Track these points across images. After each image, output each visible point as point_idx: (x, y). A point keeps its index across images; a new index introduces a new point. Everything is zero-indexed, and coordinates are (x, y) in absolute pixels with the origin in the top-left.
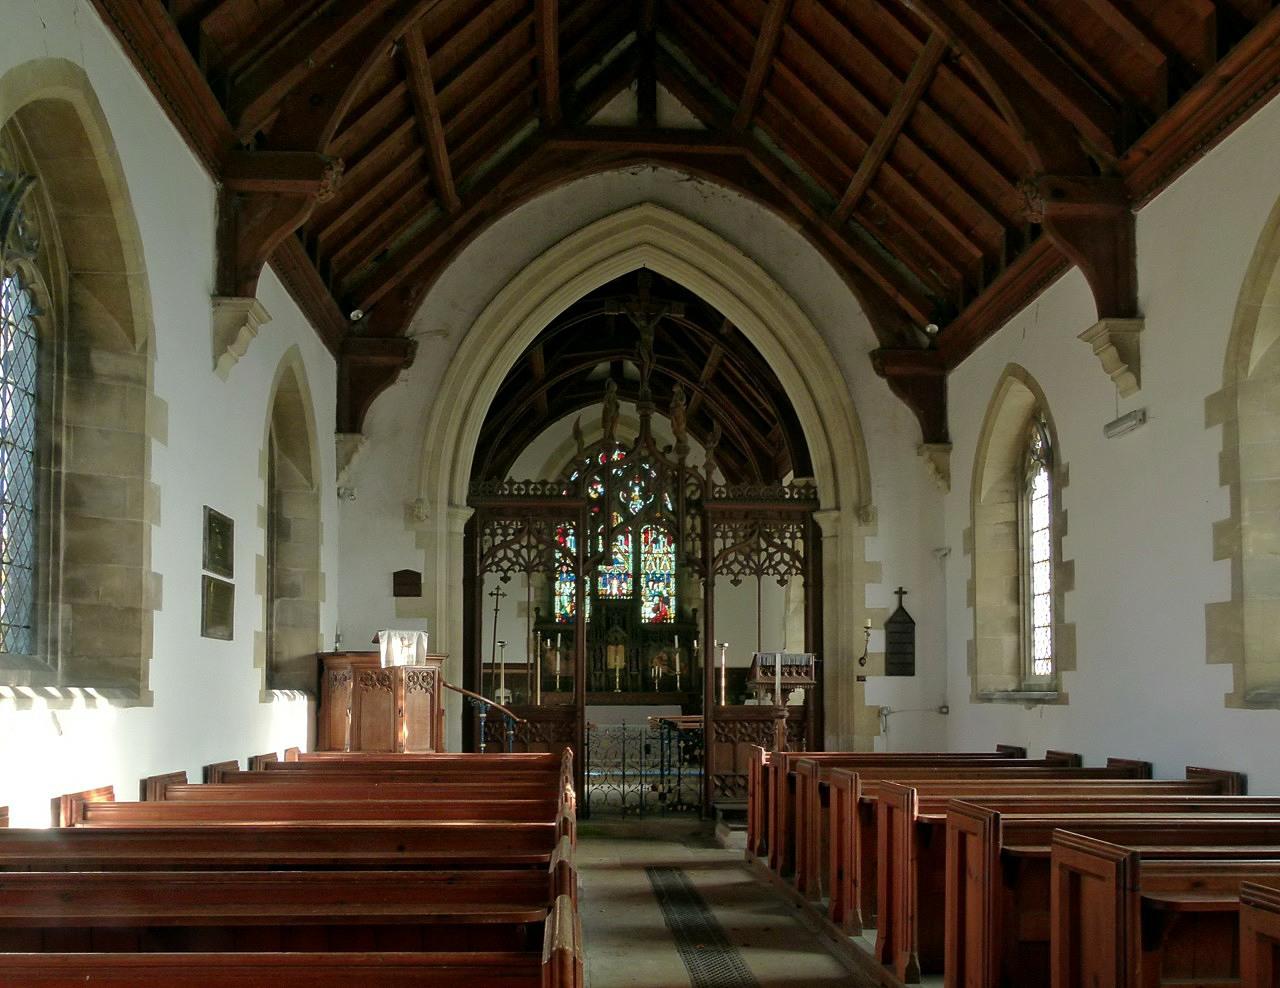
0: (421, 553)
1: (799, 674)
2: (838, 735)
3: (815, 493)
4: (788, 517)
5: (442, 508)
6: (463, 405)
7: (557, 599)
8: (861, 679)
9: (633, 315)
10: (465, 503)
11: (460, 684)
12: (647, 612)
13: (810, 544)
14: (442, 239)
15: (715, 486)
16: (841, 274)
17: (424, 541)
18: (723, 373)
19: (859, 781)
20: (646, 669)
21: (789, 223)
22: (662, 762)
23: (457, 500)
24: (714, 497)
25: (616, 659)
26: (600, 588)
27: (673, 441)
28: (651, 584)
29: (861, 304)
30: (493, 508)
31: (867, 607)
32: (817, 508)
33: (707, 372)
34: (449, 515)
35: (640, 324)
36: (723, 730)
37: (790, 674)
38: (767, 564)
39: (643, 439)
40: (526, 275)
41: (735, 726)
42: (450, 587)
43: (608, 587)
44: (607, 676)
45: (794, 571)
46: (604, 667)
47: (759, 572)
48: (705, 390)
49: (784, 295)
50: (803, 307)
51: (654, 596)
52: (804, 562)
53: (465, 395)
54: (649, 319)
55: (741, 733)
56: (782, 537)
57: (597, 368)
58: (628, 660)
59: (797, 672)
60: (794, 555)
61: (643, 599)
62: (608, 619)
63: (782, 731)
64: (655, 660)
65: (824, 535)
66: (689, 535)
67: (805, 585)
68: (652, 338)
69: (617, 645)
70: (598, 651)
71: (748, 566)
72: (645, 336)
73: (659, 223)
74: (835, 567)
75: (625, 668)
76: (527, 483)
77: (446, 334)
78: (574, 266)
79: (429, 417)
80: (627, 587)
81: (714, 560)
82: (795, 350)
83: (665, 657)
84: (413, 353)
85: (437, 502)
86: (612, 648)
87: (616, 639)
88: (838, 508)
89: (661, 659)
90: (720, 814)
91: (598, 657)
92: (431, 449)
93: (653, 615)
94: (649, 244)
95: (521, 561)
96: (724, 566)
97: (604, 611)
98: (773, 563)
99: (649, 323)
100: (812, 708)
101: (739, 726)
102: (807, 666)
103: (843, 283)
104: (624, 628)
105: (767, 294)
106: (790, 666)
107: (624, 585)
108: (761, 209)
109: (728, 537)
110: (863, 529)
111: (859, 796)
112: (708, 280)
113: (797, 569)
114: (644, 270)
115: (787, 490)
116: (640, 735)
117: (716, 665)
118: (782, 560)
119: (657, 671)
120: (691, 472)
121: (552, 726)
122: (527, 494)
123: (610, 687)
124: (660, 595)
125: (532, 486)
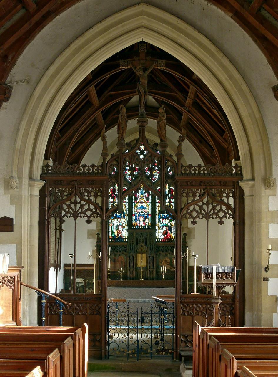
0: (13, 208)
1: (227, 278)
2: (253, 312)
3: (241, 170)
4: (225, 184)
5: (26, 181)
6: (38, 122)
7: (110, 228)
8: (266, 280)
9: (136, 68)
10: (39, 178)
11: (36, 284)
12: (160, 235)
13: (237, 200)
14: (27, 27)
15: (182, 166)
16: (255, 41)
17: (16, 201)
18: (197, 100)
19: (236, 361)
20: (158, 267)
21: (225, 12)
22: (173, 313)
23: (34, 177)
24: (182, 173)
25: (142, 262)
26: (133, 222)
27: (158, 141)
28: (161, 219)
29: (268, 59)
30: (56, 181)
31: (270, 237)
32: (242, 179)
33: (188, 102)
34: (30, 185)
35: (139, 73)
36: (186, 308)
37: (222, 278)
38: (212, 212)
39: (141, 140)
40: (73, 47)
41: (193, 306)
42: (31, 226)
43: (138, 221)
44: (136, 271)
45: (228, 216)
46: (134, 266)
47: (207, 216)
48: (189, 111)
49: (222, 55)
50: (232, 61)
51: (163, 226)
52: (234, 211)
53: (39, 116)
54: (145, 70)
55: (196, 310)
56: (221, 196)
57: (132, 100)
58: (148, 262)
59: (226, 277)
60: (228, 206)
61: (157, 228)
62: (137, 239)
63: (217, 311)
64: (163, 262)
65: (245, 195)
66: (167, 195)
67: (234, 224)
68: (146, 82)
69: (142, 253)
70: (131, 257)
71: (201, 213)
72: (141, 80)
73: (149, 15)
74: (252, 214)
75: (146, 267)
76: (93, 166)
77: (28, 82)
78: (101, 40)
79: (18, 129)
80: (148, 221)
81: (181, 209)
82: (227, 85)
83: (169, 260)
84: (10, 94)
85: (22, 178)
86: (139, 256)
87: (142, 250)
88: (253, 179)
89: (166, 261)
90: (183, 358)
91: (132, 261)
92: (19, 148)
93: (163, 237)
94: (144, 27)
95: (71, 211)
96: (187, 213)
97: (135, 235)
98: (216, 211)
99: (144, 72)
100: (237, 296)
101: (195, 306)
102: (232, 273)
103: (257, 47)
104: (146, 244)
105: (212, 55)
106: (222, 273)
107: (147, 220)
108: (209, 4)
109: (190, 196)
110: (268, 191)
111: (235, 370)
112: (178, 47)
113: (230, 214)
114: (142, 42)
115: (233, 169)
116: (138, 311)
117: (191, 265)
118: (221, 210)
119: (164, 268)
120: (168, 158)
121: (88, 305)
122: (84, 172)
123: (138, 277)
124: (167, 226)
125: (96, 168)
